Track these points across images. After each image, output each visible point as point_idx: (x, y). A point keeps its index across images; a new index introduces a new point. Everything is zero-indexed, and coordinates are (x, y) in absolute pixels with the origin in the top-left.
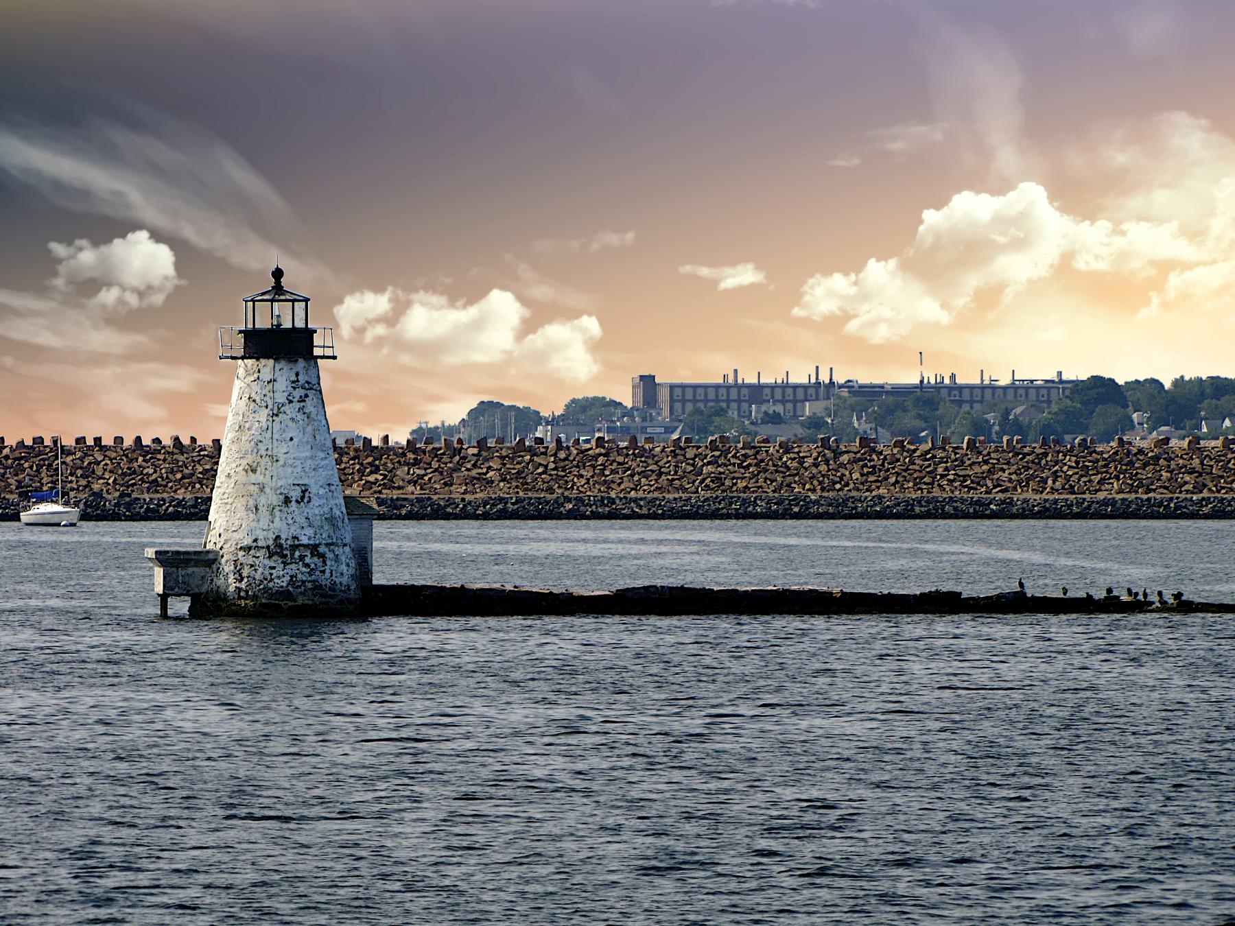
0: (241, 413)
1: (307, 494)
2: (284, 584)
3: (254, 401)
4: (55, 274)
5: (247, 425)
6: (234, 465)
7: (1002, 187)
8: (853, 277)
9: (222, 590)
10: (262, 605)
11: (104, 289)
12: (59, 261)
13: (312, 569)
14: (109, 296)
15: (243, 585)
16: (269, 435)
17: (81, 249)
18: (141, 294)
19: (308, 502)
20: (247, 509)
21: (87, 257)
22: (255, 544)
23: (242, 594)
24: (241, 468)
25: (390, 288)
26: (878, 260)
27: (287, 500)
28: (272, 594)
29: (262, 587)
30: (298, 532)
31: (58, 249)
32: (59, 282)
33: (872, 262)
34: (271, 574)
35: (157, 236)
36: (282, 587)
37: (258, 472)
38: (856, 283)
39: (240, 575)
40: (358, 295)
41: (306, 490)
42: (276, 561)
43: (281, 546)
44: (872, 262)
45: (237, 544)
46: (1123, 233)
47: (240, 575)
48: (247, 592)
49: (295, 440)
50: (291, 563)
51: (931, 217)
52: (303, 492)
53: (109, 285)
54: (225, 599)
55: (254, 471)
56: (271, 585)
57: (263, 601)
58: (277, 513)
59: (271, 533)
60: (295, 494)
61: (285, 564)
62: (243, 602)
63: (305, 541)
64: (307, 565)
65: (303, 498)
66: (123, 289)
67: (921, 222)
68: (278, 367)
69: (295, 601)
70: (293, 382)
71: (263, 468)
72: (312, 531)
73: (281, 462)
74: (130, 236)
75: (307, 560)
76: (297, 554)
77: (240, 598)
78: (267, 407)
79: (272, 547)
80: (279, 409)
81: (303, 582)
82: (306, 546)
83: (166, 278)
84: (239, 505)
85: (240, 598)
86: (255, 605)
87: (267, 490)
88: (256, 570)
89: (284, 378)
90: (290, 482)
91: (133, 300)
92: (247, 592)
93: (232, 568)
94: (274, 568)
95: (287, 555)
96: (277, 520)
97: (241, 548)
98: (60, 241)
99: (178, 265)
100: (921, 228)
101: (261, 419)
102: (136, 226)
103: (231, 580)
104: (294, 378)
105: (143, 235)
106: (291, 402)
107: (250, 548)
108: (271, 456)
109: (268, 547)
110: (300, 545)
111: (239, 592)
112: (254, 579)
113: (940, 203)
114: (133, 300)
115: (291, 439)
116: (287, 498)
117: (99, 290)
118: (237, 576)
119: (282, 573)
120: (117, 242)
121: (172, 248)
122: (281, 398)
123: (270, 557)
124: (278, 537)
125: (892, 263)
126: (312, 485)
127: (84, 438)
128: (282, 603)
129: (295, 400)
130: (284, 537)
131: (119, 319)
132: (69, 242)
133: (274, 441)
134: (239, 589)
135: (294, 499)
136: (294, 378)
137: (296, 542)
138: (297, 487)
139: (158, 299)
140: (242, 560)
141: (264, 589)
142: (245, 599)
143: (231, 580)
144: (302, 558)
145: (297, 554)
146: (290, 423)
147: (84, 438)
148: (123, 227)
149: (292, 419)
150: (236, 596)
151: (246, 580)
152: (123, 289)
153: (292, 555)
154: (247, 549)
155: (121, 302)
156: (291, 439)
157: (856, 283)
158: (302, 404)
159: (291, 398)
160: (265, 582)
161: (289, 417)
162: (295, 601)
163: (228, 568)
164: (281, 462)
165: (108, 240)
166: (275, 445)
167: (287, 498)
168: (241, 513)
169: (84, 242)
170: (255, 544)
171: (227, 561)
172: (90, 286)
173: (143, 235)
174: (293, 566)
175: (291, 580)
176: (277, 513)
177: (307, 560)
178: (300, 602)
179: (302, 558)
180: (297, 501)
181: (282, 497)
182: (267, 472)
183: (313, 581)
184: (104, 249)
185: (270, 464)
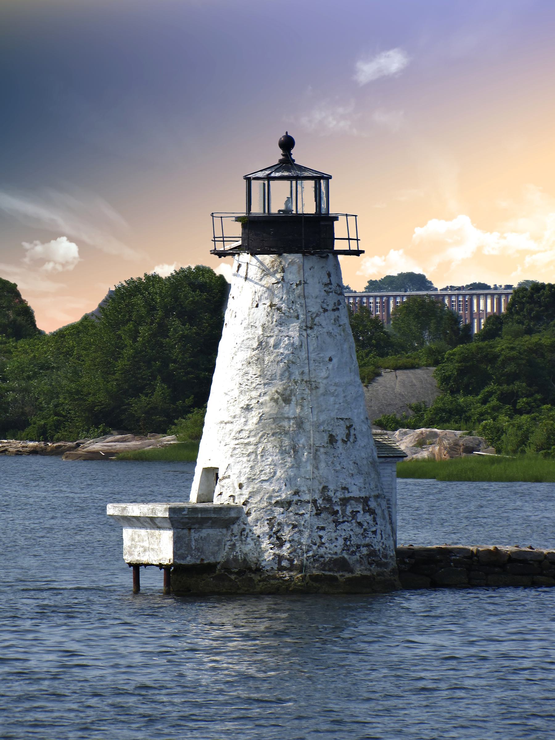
0: (258, 324)
1: (352, 432)
2: (339, 552)
3: (279, 309)
4: (25, 256)
5: (272, 341)
6: (254, 394)
7: (450, 218)
8: (383, 258)
9: (252, 558)
10: (315, 578)
11: (47, 263)
12: (27, 250)
13: (365, 530)
14: (49, 266)
15: (285, 551)
16: (303, 355)
17: (36, 245)
18: (63, 265)
19: (355, 442)
20: (283, 452)
21: (39, 248)
22: (296, 498)
23: (284, 563)
24: (267, 398)
25: (175, 263)
26: (395, 250)
27: (332, 440)
28: (324, 564)
29: (311, 554)
30: (347, 481)
31: (26, 245)
32: (27, 260)
33: (392, 251)
34: (321, 537)
35: (71, 239)
36: (336, 553)
37: (293, 403)
38: (385, 260)
39: (278, 538)
40: (161, 266)
41: (351, 426)
42: (326, 519)
43: (328, 500)
44: (392, 251)
45: (270, 498)
46: (505, 238)
47: (278, 538)
48: (291, 561)
49: (335, 360)
50: (344, 522)
51: (419, 231)
52: (349, 428)
53: (49, 261)
54: (258, 570)
55: (287, 401)
56: (322, 551)
57: (315, 572)
58: (322, 457)
59: (317, 483)
60: (340, 432)
61: (337, 523)
62: (286, 575)
63: (355, 492)
64: (360, 524)
65: (348, 435)
66: (55, 263)
67: (414, 233)
68: (308, 265)
69: (352, 571)
70: (326, 285)
71: (299, 397)
72: (362, 480)
73: (321, 390)
74: (58, 239)
75: (360, 518)
76: (349, 509)
77: (281, 569)
78: (298, 317)
79: (320, 501)
80: (313, 319)
81: (358, 547)
82: (357, 499)
83: (74, 258)
84: (269, 445)
85: (281, 569)
86: (304, 578)
87: (307, 426)
88: (300, 532)
89: (316, 280)
90: (333, 414)
91: (59, 268)
92: (291, 561)
93: (266, 529)
94: (323, 529)
95: (338, 511)
96: (322, 465)
97: (277, 502)
98: (27, 242)
99: (80, 252)
100: (414, 236)
101: (291, 333)
102: (62, 235)
103: (265, 544)
104: (326, 280)
105: (64, 239)
106: (325, 310)
107: (289, 503)
108: (308, 382)
109: (315, 502)
110: (351, 498)
111: (280, 562)
112: (300, 543)
113: (422, 224)
114: (59, 268)
115: (331, 360)
116: (331, 436)
117: (44, 264)
118: (274, 539)
119: (334, 535)
120: (53, 242)
121: (77, 245)
122: (314, 308)
123: (317, 514)
124: (325, 488)
125: (401, 252)
126: (355, 419)
127: (218, 468)
128: (337, 575)
129: (330, 308)
130: (331, 487)
131: (52, 276)
132: (31, 242)
133: (312, 362)
134: (280, 558)
135: (339, 438)
136: (326, 280)
137: (347, 495)
138: (342, 422)
139: (71, 267)
140: (281, 518)
141: (313, 556)
142: (290, 569)
143: (265, 544)
144: (354, 514)
145: (349, 509)
146: (328, 340)
147: (218, 468)
148: (55, 235)
149: (329, 334)
150: (276, 567)
151: (288, 545)
152: (55, 263)
153: (344, 511)
154: (286, 504)
155: (54, 269)
156: (331, 360)
157: (385, 260)
158: (336, 313)
159: (325, 306)
160: (315, 548)
161: (325, 330)
162: (352, 571)
163: (261, 529)
164: (321, 390)
165: (49, 241)
166: (312, 368)
167: (331, 436)
168: (273, 457)
169: (37, 242)
170: (296, 498)
171: (257, 520)
172: (41, 261)
173: (64, 239)
174: (345, 526)
175: (345, 544)
176: (322, 457)
177: (360, 518)
178: (358, 572)
179: (354, 514)
180: (344, 442)
181: (326, 438)
182: (305, 403)
183: (367, 545)
184: (46, 245)
185: (307, 391)
